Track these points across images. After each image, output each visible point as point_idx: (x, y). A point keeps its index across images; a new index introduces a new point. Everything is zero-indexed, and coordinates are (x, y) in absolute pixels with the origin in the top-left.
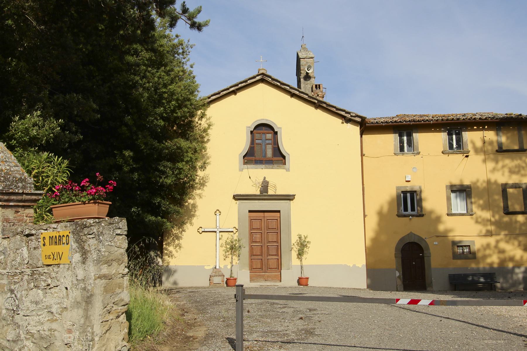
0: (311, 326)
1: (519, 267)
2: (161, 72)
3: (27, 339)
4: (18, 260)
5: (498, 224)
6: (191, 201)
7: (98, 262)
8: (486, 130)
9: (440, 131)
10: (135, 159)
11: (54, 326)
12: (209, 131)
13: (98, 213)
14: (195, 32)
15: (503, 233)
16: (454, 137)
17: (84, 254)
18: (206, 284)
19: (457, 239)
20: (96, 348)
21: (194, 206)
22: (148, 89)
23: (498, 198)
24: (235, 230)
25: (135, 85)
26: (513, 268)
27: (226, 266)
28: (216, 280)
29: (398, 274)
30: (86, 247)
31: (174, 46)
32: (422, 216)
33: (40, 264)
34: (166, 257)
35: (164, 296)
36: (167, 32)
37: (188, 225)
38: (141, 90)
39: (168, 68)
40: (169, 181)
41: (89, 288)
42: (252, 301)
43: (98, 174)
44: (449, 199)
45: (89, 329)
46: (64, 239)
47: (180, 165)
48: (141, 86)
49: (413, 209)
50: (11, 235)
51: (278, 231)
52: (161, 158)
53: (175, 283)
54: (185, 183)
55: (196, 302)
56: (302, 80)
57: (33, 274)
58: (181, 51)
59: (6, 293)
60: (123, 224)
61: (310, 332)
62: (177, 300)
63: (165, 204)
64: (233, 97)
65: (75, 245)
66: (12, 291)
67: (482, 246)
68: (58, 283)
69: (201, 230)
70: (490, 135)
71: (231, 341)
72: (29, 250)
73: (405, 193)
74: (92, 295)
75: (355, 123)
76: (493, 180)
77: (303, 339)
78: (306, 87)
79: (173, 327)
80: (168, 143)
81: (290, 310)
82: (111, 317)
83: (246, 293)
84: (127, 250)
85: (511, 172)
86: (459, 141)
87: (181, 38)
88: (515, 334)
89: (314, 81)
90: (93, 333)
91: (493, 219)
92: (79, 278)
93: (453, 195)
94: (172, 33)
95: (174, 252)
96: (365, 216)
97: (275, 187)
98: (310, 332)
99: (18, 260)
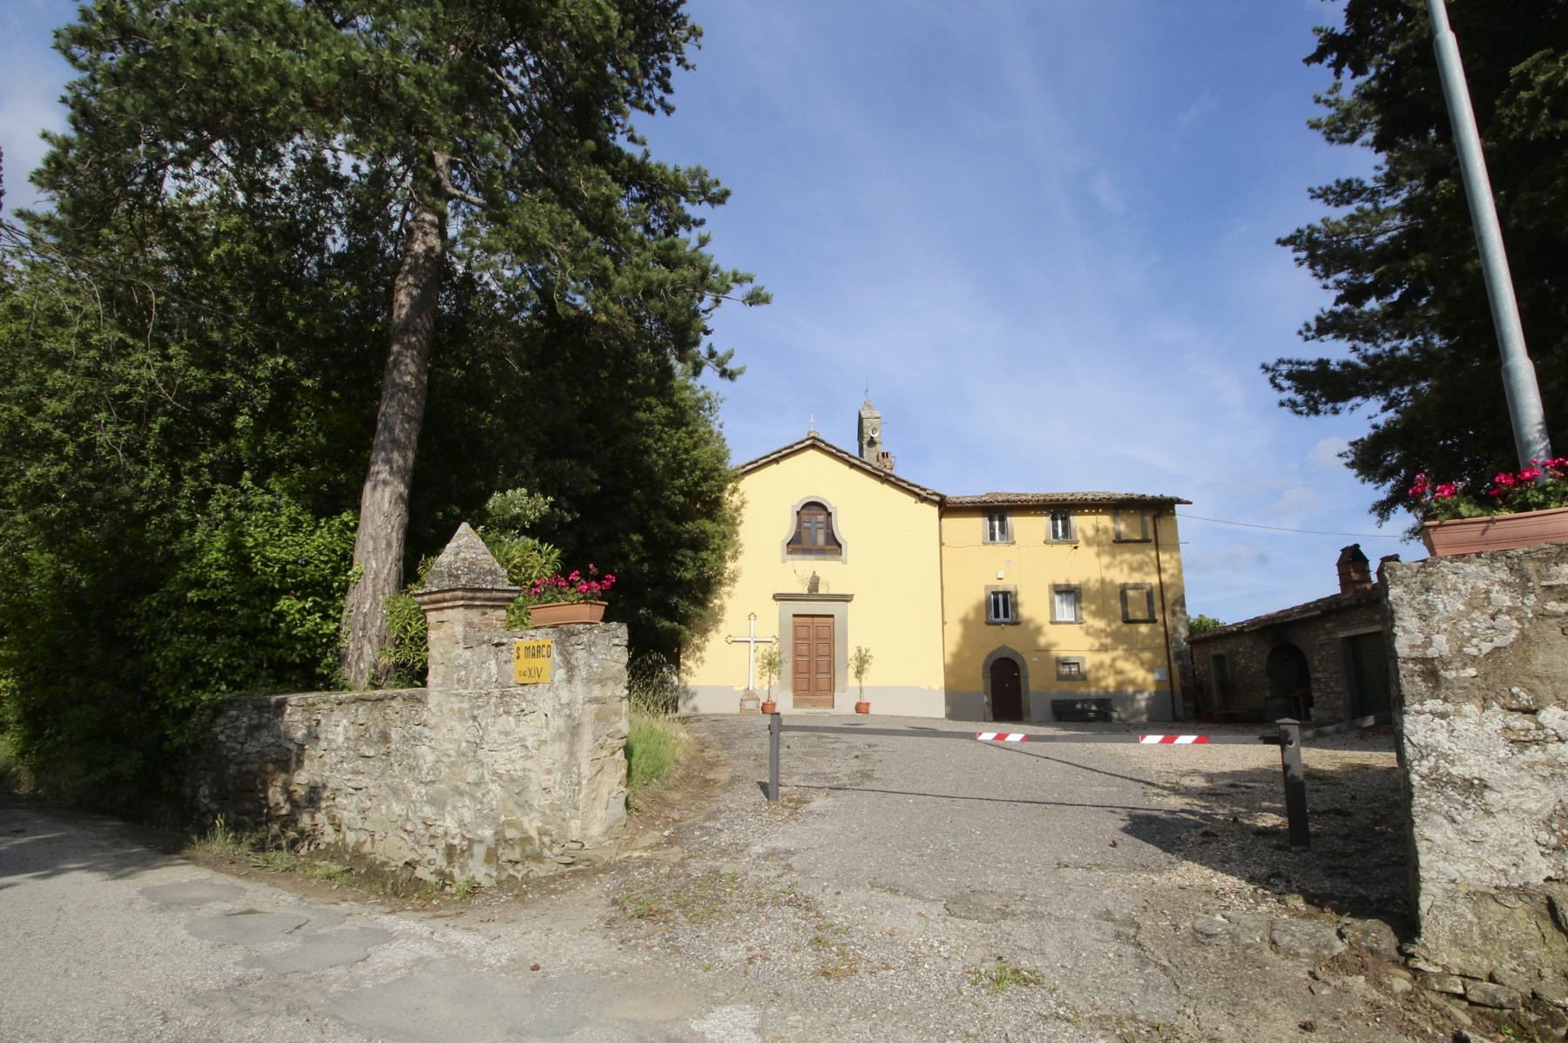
0: (869, 767)
1: (1141, 692)
2: (682, 433)
3: (493, 781)
4: (484, 676)
5: (1117, 637)
6: (717, 602)
7: (589, 681)
8: (1102, 514)
9: (1042, 515)
10: (644, 545)
11: (529, 764)
12: (743, 511)
13: (590, 618)
14: (726, 381)
15: (1121, 647)
16: (1060, 522)
17: (571, 669)
18: (736, 710)
19: (1063, 654)
20: (583, 794)
21: (722, 608)
22: (663, 455)
23: (1116, 604)
24: (774, 640)
25: (647, 450)
26: (1135, 692)
27: (762, 687)
28: (750, 705)
29: (986, 699)
30: (573, 662)
31: (699, 400)
32: (1017, 623)
33: (512, 682)
34: (683, 675)
35: (678, 725)
36: (691, 381)
37: (713, 632)
38: (654, 456)
39: (690, 428)
40: (688, 575)
41: (576, 715)
42: (791, 733)
43: (591, 566)
44: (1052, 603)
45: (575, 770)
46: (545, 650)
47: (704, 555)
48: (655, 451)
49: (1006, 615)
50: (474, 644)
51: (830, 642)
52: (679, 544)
53: (695, 709)
54: (710, 578)
55: (721, 733)
56: (865, 446)
57: (503, 695)
58: (707, 406)
59: (467, 720)
60: (621, 632)
61: (867, 776)
62: (696, 732)
63: (684, 606)
64: (774, 467)
65: (558, 659)
66: (475, 718)
67: (1094, 665)
68: (536, 708)
69: (730, 640)
70: (1105, 521)
71: (763, 787)
72: (498, 663)
73: (996, 593)
74: (579, 725)
75: (932, 502)
76: (1108, 579)
77: (857, 784)
78: (870, 455)
79: (688, 767)
80: (689, 526)
81: (843, 746)
82: (604, 753)
83: (784, 723)
84: (628, 667)
85: (1132, 569)
86: (1066, 528)
87: (707, 390)
88: (1132, 779)
89: (880, 449)
90: (579, 774)
91: (1108, 629)
92: (563, 701)
93: (1057, 598)
94: (696, 383)
95: (694, 669)
96: (944, 623)
97: (827, 584)
98: (867, 776)
99: (484, 676)
